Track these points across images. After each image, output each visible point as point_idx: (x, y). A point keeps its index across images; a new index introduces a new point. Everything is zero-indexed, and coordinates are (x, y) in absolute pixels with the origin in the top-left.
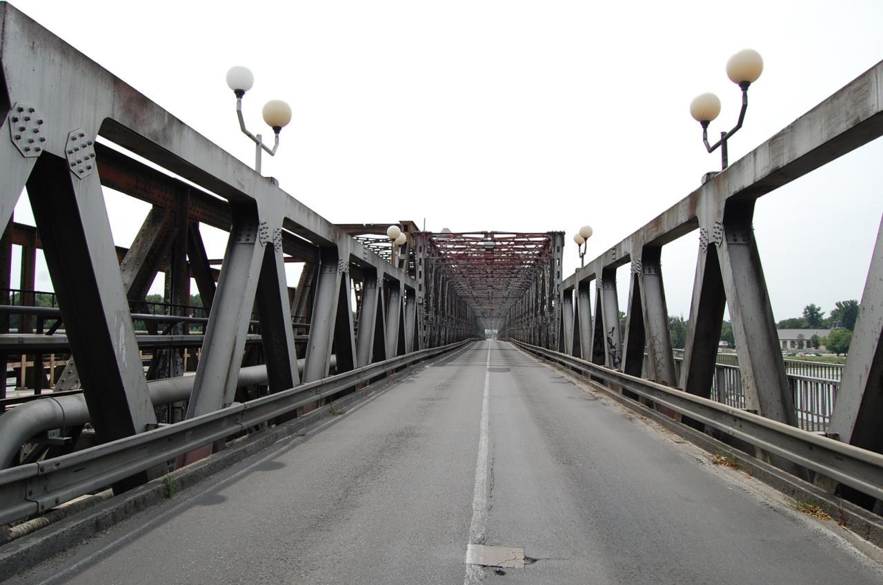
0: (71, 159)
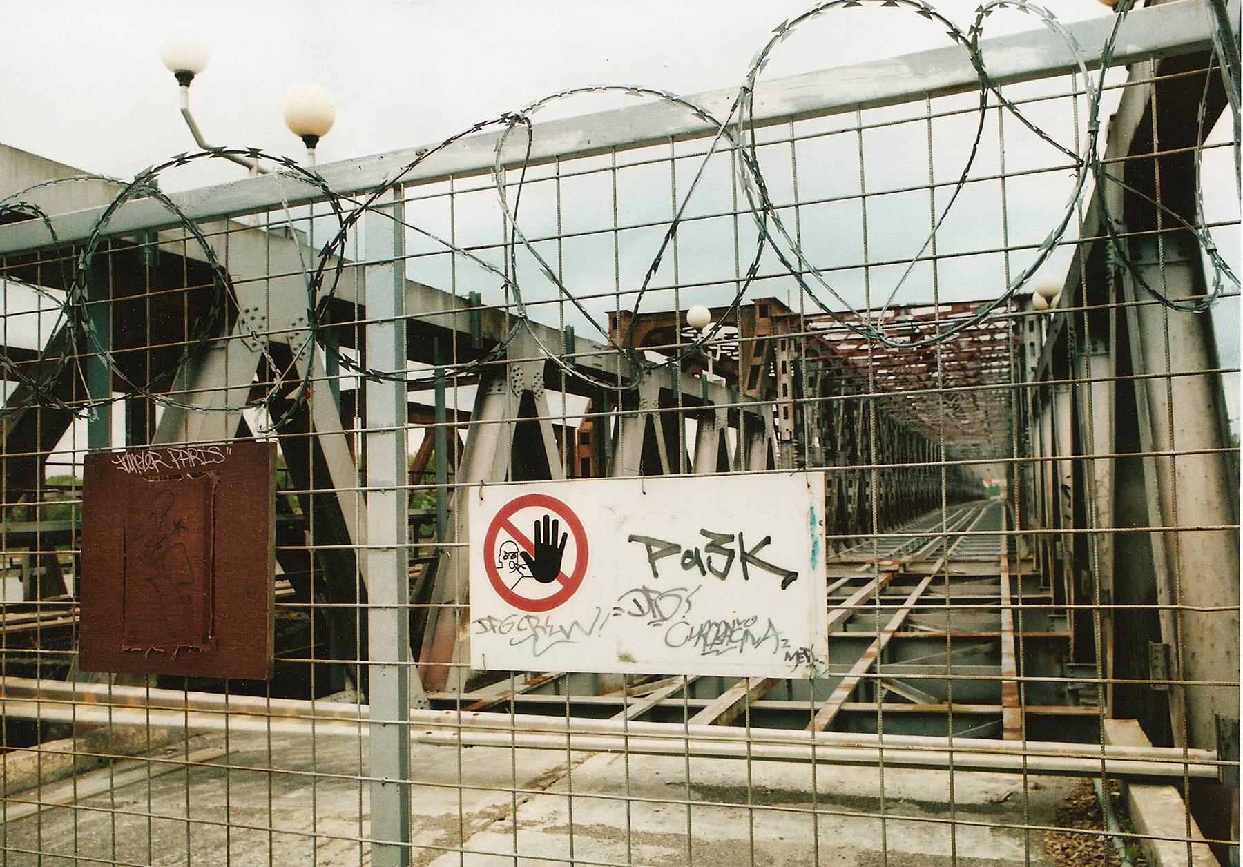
0: (294, 344)
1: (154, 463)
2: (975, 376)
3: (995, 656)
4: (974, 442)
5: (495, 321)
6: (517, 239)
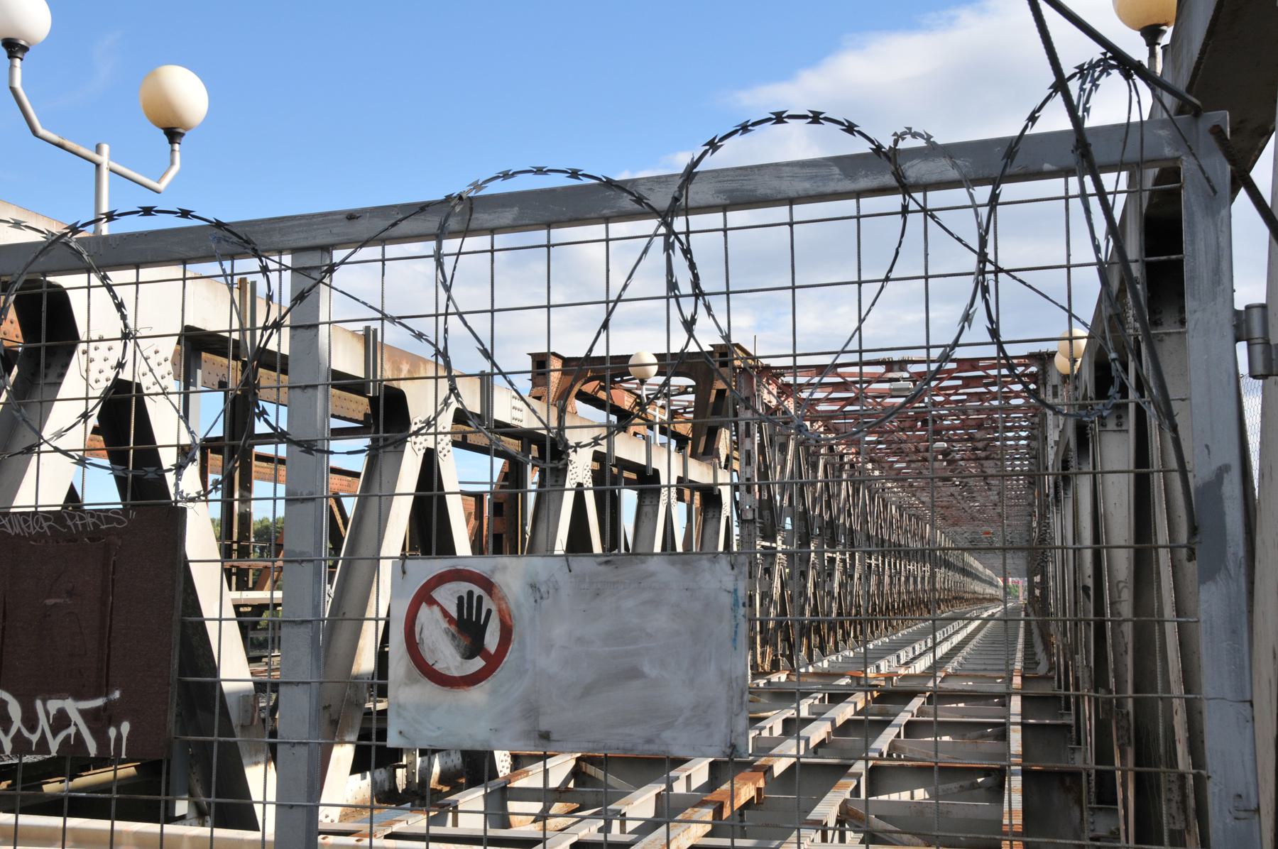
1: (45, 525)
2: (984, 449)
3: (997, 790)
4: (985, 528)
5: (393, 363)
6: (452, 309)
